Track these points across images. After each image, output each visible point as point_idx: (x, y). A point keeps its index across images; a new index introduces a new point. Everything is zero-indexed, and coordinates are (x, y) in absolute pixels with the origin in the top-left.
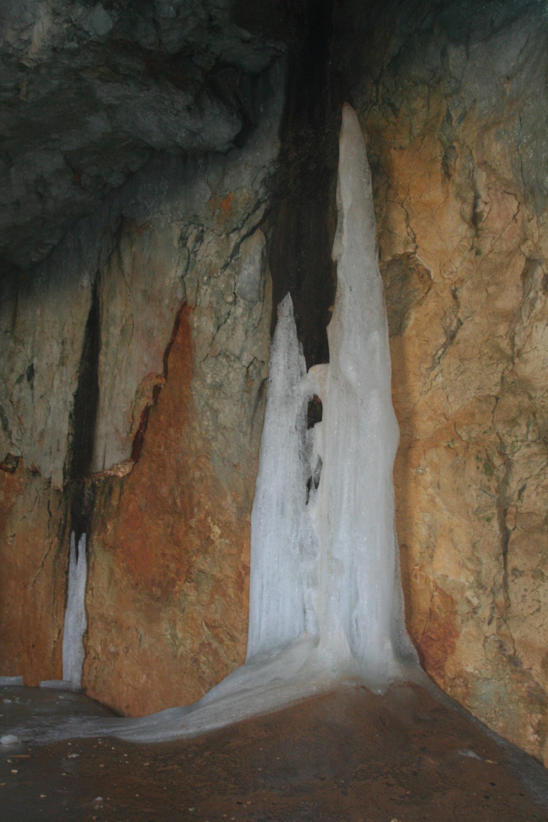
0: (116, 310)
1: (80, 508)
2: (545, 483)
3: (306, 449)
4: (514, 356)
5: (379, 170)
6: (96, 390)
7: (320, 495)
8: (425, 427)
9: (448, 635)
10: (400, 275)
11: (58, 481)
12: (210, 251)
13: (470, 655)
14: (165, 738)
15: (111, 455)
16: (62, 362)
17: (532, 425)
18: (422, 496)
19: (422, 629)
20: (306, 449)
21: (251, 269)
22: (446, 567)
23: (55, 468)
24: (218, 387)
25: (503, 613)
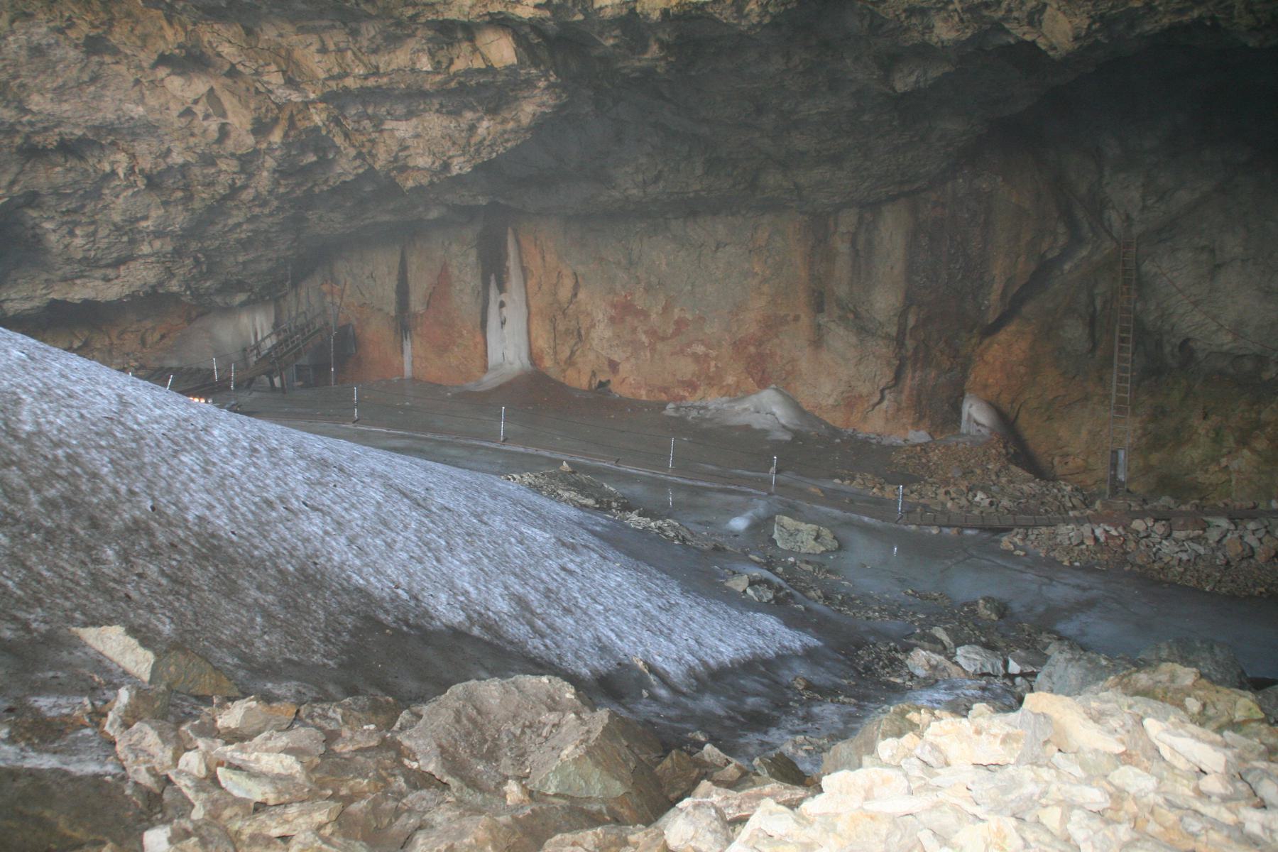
0: (414, 262)
1: (403, 324)
2: (970, 836)
3: (501, 313)
4: (555, 294)
5: (518, 242)
6: (407, 286)
7: (507, 327)
8: (533, 309)
9: (541, 358)
10: (524, 270)
11: (393, 313)
12: (455, 248)
13: (548, 363)
14: (101, 653)
15: (416, 304)
16: (389, 274)
17: (171, 586)
18: (533, 327)
19: (534, 357)
20: (501, 313)
21: (473, 257)
22: (542, 343)
23: (392, 309)
24: (461, 291)
25: (555, 353)
